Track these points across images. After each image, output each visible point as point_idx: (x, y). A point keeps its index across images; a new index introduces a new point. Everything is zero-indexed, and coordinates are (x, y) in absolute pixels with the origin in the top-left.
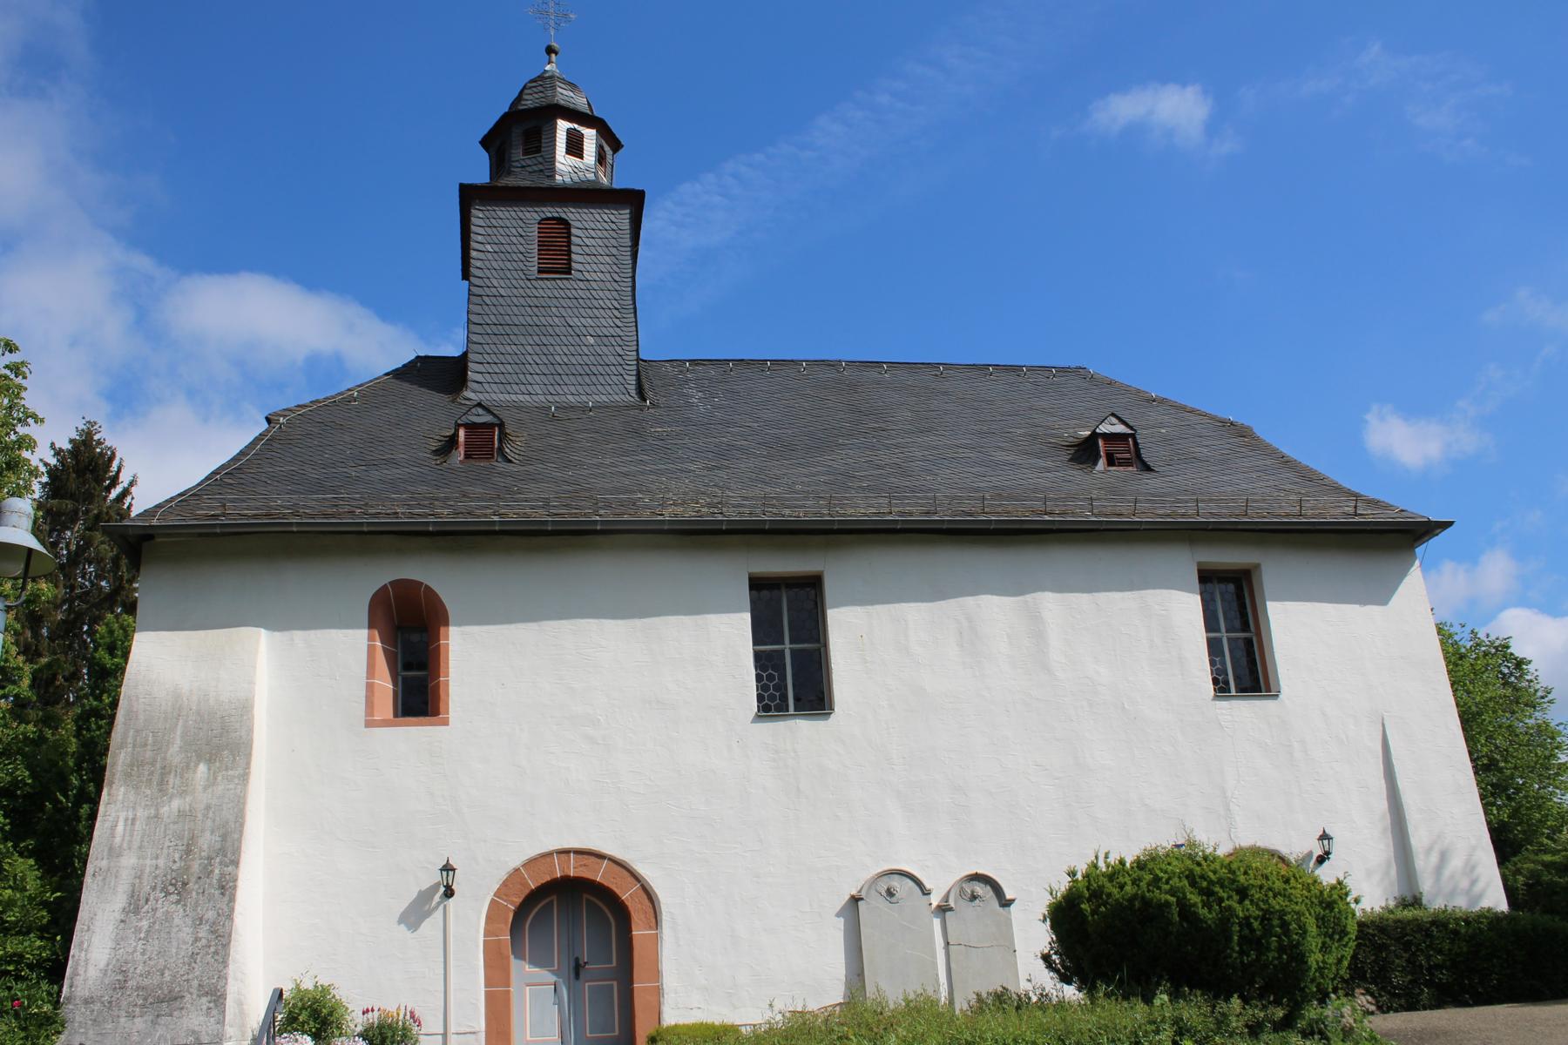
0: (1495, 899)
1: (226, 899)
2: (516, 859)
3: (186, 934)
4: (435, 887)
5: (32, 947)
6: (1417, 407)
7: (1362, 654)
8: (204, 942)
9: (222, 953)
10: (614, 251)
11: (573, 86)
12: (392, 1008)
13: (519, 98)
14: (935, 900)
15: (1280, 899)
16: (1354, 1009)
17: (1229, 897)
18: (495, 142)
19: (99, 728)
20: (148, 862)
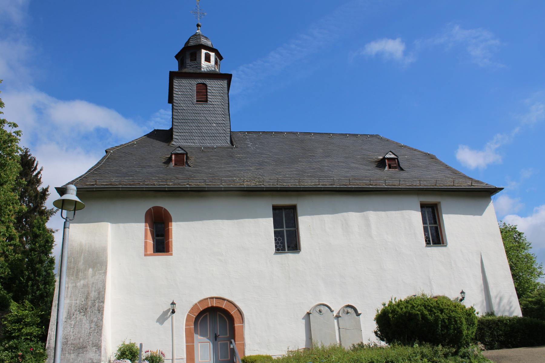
0: (518, 312)
1: (100, 314)
2: (196, 301)
3: (87, 326)
4: (169, 310)
5: (35, 330)
6: (477, 145)
7: (472, 232)
8: (93, 328)
9: (99, 332)
10: (222, 95)
11: (206, 38)
12: (155, 350)
13: (188, 42)
14: (335, 314)
15: (454, 313)
16: (478, 349)
17: (438, 312)
18: (180, 57)
19: (35, 255)
20: (73, 302)
